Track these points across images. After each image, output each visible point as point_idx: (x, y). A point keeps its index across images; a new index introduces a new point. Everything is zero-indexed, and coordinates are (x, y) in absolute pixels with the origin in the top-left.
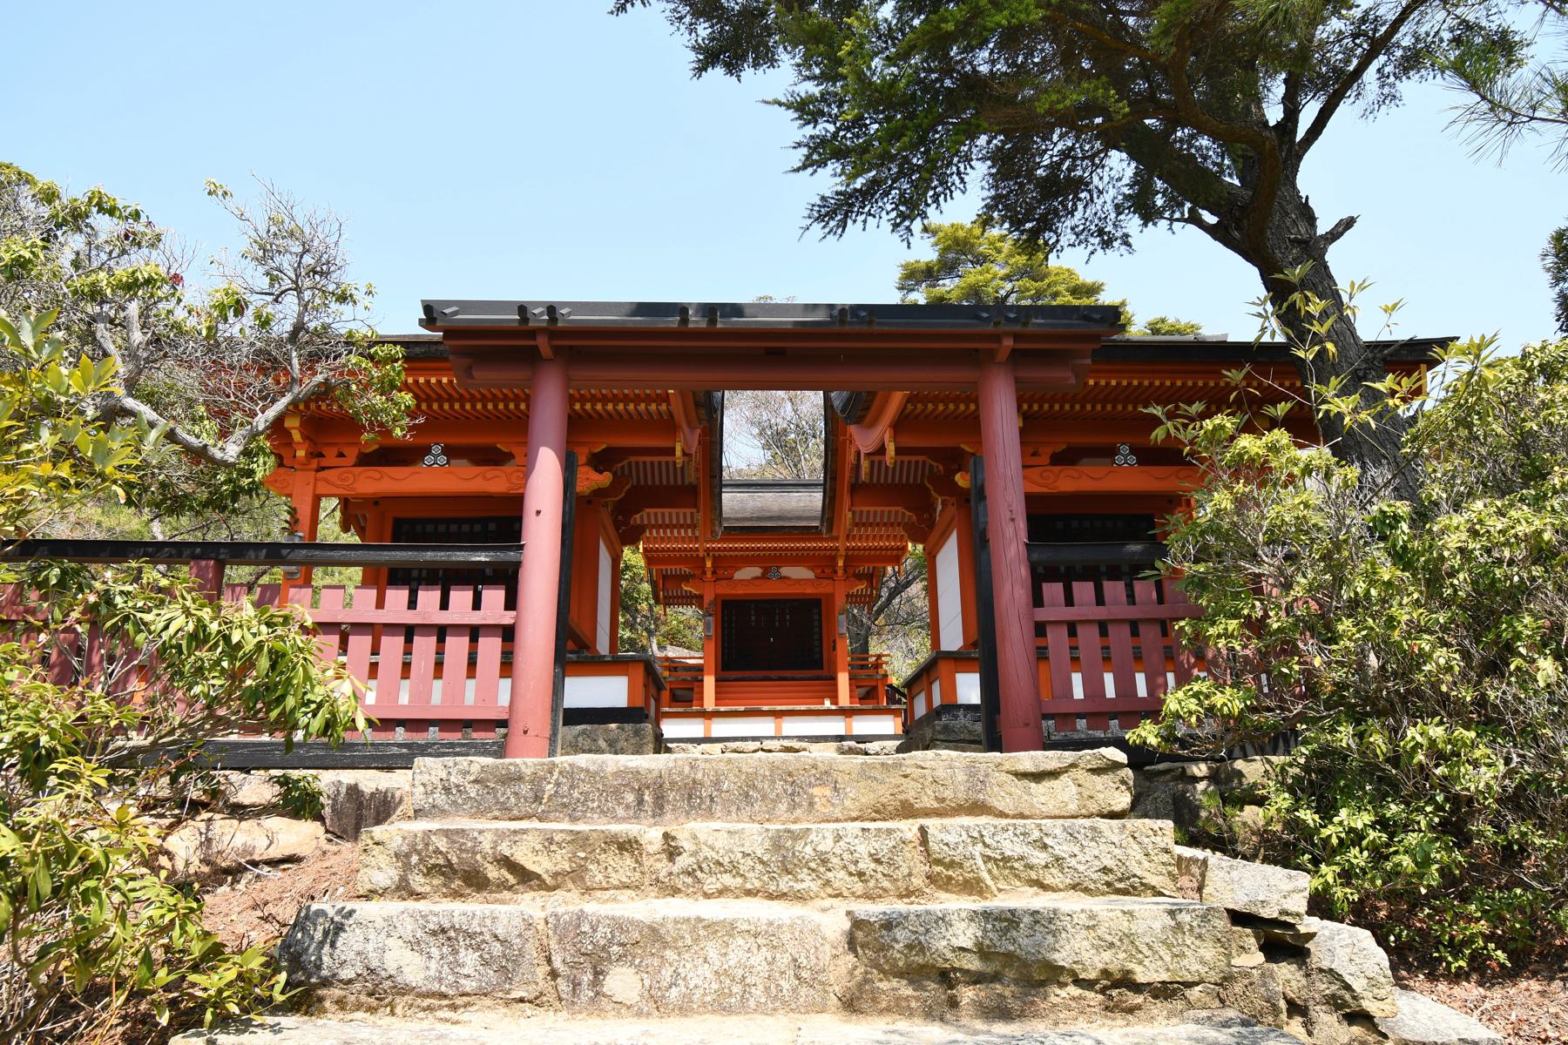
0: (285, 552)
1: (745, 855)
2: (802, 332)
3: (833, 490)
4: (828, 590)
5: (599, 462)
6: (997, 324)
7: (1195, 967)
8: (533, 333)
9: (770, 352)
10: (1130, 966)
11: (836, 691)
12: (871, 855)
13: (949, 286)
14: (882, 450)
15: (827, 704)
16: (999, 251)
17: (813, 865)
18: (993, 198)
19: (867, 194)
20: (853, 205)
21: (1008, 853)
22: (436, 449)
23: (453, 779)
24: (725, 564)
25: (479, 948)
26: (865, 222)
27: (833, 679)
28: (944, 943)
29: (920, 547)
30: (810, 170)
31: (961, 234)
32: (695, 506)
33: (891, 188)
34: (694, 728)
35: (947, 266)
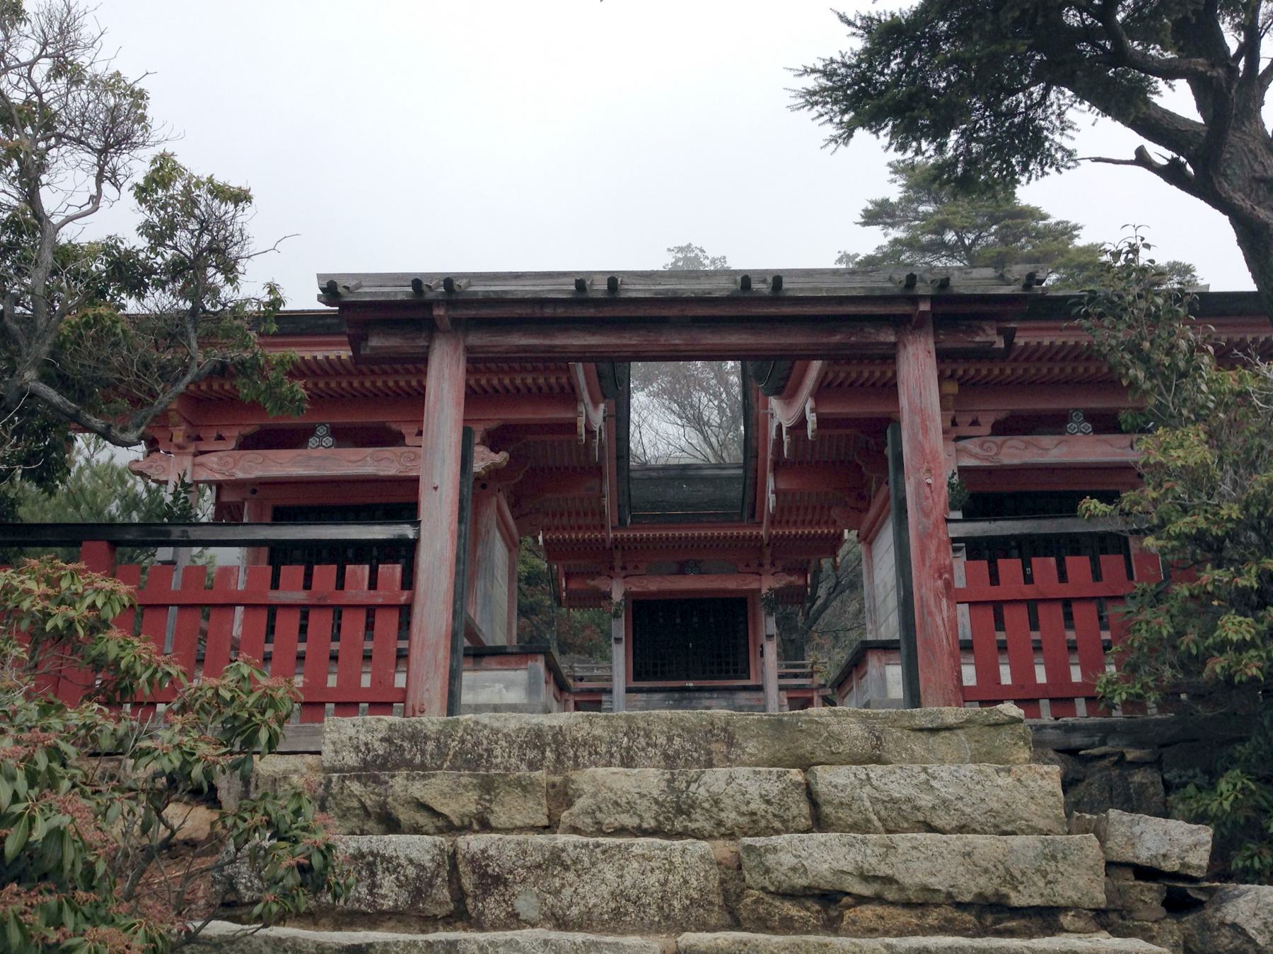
1: (642, 796)
5: (495, 441)
7: (1070, 893)
8: (430, 305)
10: (1004, 890)
12: (761, 796)
14: (802, 422)
17: (706, 805)
21: (896, 795)
22: (321, 431)
23: (361, 737)
25: (395, 871)
28: (826, 866)
29: (855, 532)
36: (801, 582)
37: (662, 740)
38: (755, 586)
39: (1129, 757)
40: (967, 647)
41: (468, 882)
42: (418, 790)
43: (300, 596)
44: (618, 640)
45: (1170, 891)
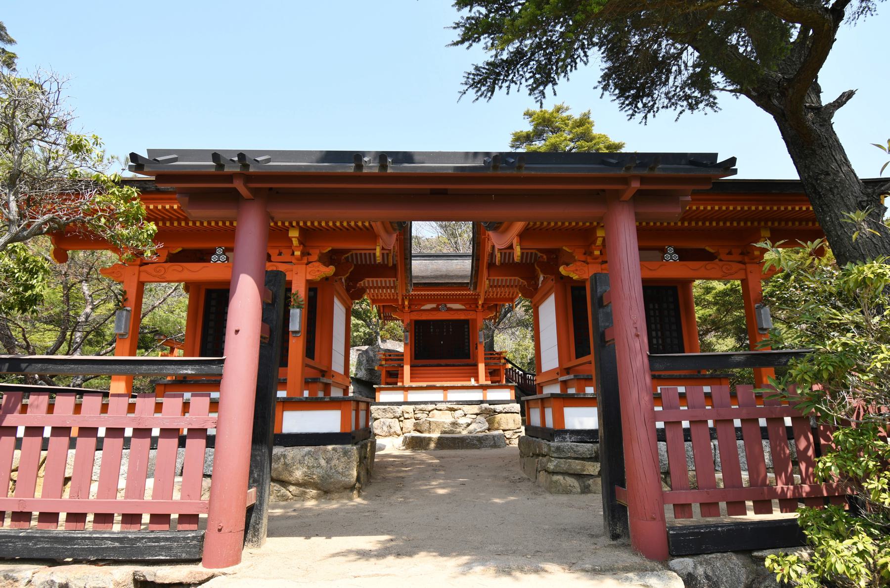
0: (23, 366)
2: (462, 176)
3: (478, 260)
4: (473, 317)
6: (628, 169)
8: (230, 177)
9: (434, 192)
11: (477, 373)
13: (539, 145)
15: (473, 382)
16: (567, 125)
18: (608, 69)
19: (511, 64)
20: (499, 74)
22: (219, 251)
24: (415, 302)
26: (508, 87)
27: (476, 366)
30: (467, 44)
31: (547, 115)
32: (395, 276)
33: (530, 59)
34: (398, 396)
35: (538, 134)
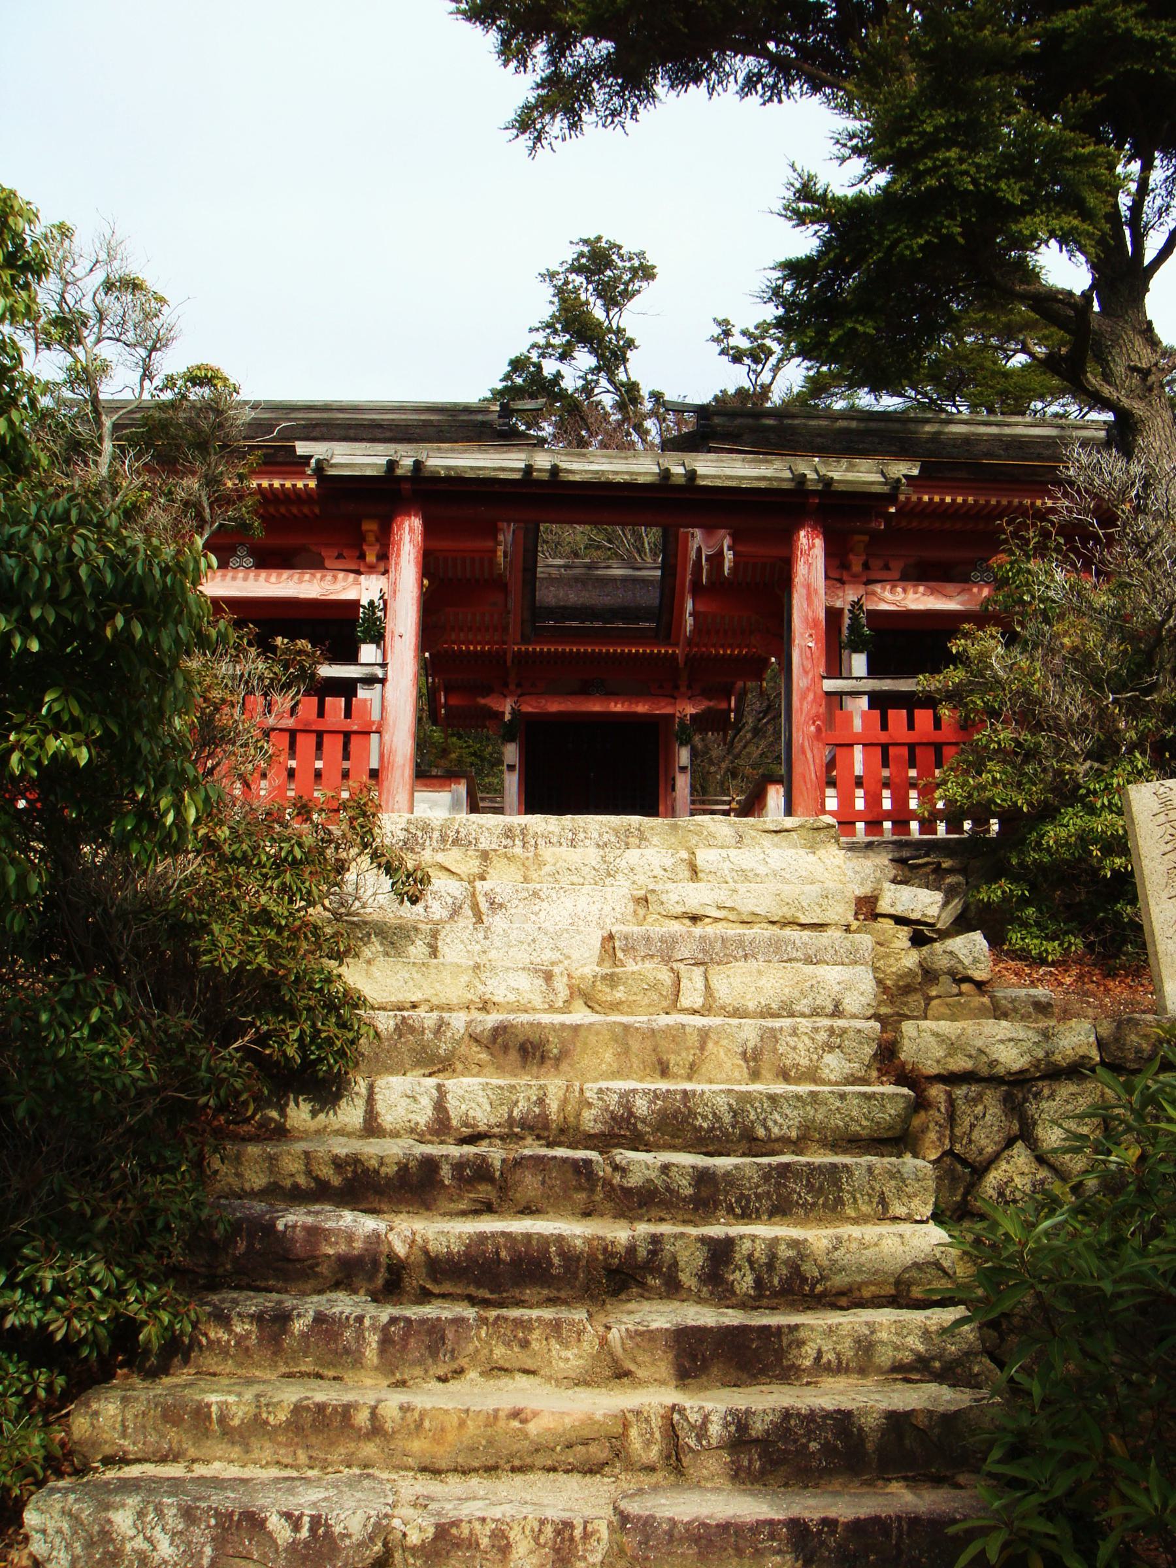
36: (724, 706)
37: (595, 835)
38: (668, 710)
39: (944, 866)
40: (859, 782)
41: (484, 906)
42: (440, 858)
43: (290, 723)
44: (511, 768)
45: (915, 931)
